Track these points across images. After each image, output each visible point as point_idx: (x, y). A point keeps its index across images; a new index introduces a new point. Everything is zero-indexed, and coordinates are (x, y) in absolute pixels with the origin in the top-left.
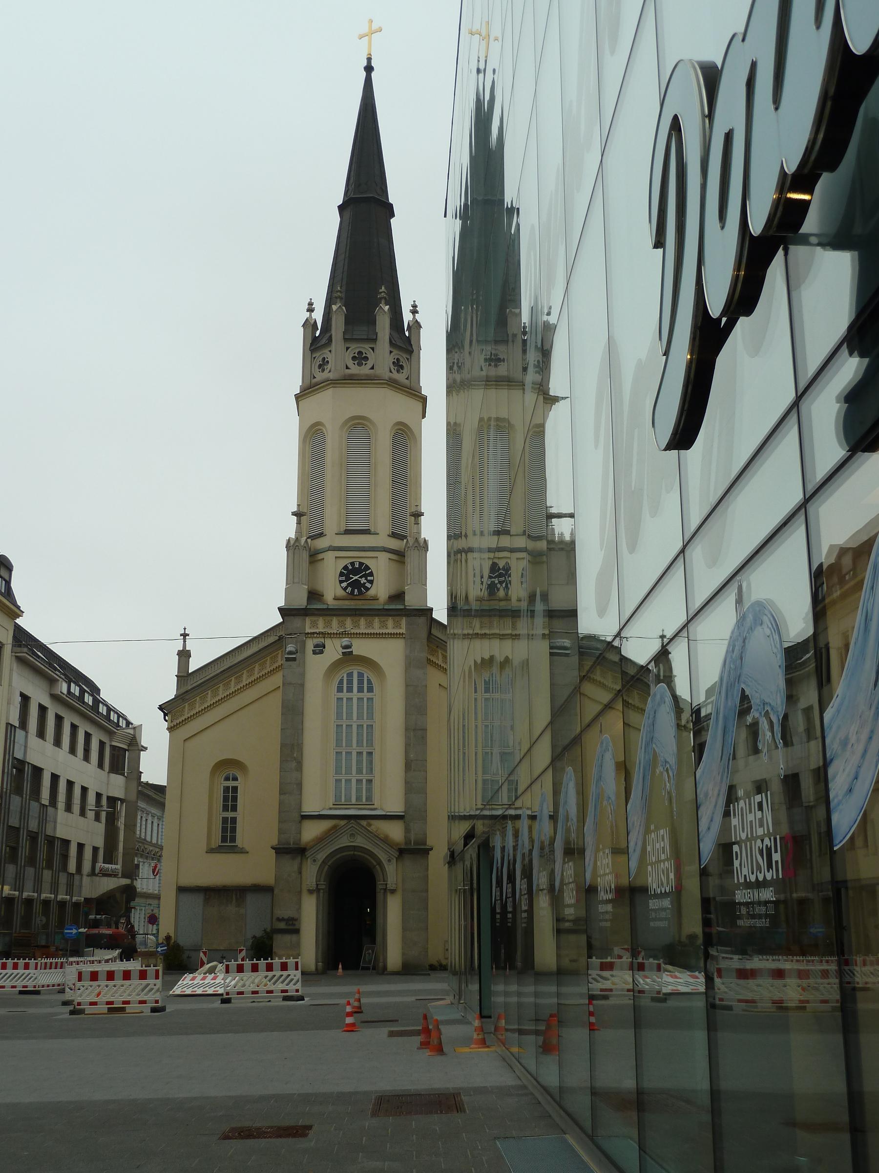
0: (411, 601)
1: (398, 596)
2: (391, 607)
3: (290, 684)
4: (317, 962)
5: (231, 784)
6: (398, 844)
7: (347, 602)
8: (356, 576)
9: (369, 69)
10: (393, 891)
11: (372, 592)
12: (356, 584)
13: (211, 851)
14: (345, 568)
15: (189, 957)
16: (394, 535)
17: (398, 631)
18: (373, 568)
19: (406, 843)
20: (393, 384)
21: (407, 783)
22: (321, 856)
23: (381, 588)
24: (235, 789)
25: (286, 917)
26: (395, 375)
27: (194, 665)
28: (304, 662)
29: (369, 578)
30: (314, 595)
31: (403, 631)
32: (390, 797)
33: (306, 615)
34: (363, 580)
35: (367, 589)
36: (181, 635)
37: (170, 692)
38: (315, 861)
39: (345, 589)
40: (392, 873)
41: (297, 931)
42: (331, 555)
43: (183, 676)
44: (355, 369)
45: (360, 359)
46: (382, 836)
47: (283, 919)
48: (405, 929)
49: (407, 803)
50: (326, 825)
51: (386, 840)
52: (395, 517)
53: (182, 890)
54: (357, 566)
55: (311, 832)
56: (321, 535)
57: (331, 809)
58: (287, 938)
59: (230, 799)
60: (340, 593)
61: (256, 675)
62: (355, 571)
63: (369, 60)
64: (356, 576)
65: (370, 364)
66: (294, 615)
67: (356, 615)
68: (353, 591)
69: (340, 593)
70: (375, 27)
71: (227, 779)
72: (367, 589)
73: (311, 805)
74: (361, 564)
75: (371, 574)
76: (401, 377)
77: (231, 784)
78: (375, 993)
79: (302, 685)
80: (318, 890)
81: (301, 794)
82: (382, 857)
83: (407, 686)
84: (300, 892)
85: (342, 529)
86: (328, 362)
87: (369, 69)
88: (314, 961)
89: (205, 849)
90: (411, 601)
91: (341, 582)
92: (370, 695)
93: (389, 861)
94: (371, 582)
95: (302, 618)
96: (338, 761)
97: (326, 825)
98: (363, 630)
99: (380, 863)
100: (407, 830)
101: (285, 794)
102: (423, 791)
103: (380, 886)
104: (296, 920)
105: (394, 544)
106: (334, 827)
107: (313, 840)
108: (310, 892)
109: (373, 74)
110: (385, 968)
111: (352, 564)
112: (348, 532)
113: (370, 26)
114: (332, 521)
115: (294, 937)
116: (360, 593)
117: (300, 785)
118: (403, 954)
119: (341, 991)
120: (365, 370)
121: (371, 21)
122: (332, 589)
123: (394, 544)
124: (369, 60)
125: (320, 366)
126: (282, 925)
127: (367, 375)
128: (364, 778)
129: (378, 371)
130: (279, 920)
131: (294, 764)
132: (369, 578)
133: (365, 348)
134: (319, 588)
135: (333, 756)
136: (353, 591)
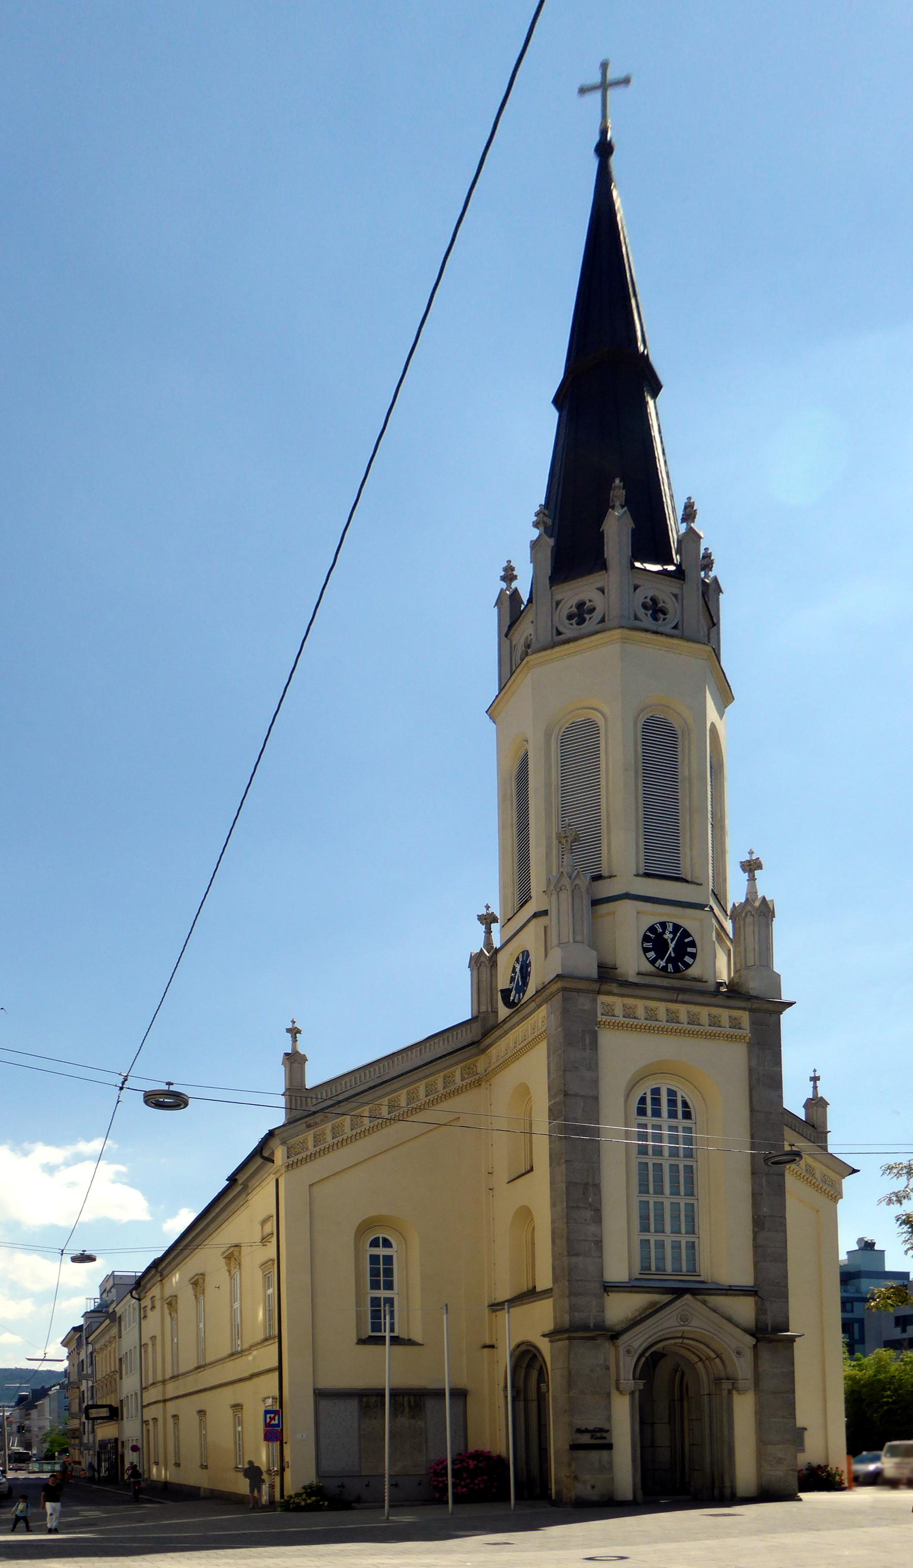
3: (576, 1095)
5: (381, 1251)
9: (604, 149)
13: (361, 1342)
24: (389, 1260)
25: (591, 1428)
27: (313, 1077)
28: (597, 1064)
29: (660, 930)
35: (688, 966)
36: (288, 1030)
38: (628, 1352)
39: (653, 962)
41: (609, 1447)
43: (296, 1093)
47: (586, 1431)
49: (756, 1278)
53: (320, 1395)
55: (619, 1308)
58: (594, 1455)
59: (381, 1272)
69: (647, 967)
70: (611, 75)
71: (375, 1243)
77: (381, 1251)
79: (596, 1098)
81: (601, 1257)
83: (752, 1110)
85: (641, 872)
87: (604, 149)
88: (631, 1491)
89: (355, 1340)
91: (646, 950)
92: (687, 1123)
100: (760, 1311)
101: (577, 1255)
104: (607, 1431)
115: (605, 1453)
126: (585, 1439)
128: (684, 1240)
130: (579, 1431)
132: (660, 930)
134: (609, 960)
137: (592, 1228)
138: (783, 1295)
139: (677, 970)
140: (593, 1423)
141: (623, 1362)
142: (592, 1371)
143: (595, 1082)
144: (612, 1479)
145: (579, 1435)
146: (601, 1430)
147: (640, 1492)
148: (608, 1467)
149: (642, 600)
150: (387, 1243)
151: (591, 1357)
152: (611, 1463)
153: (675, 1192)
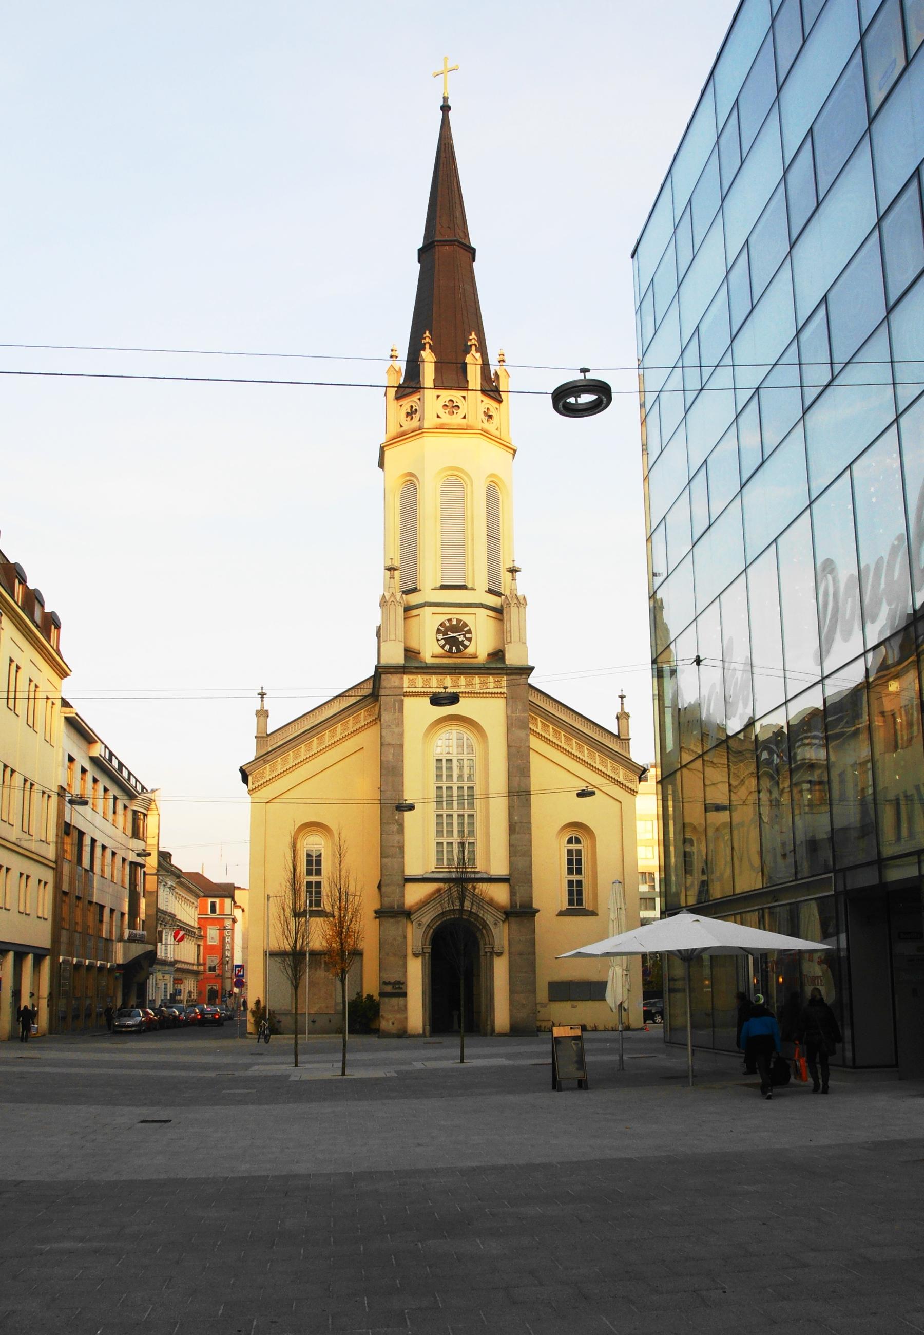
0: (512, 659)
1: (498, 655)
2: (494, 666)
3: (389, 744)
4: (424, 1026)
5: (574, 847)
6: (503, 907)
7: (445, 661)
8: (454, 636)
9: (445, 108)
10: (499, 954)
11: (470, 650)
12: (452, 642)
14: (442, 624)
15: (279, 1022)
16: (490, 591)
17: (499, 690)
18: (472, 626)
19: (512, 906)
20: (485, 433)
21: (511, 845)
22: (427, 919)
23: (480, 646)
25: (393, 981)
26: (487, 426)
29: (467, 636)
30: (410, 653)
31: (504, 690)
32: (494, 858)
33: (404, 673)
34: (461, 638)
35: (466, 647)
37: (249, 753)
38: (420, 924)
39: (443, 647)
40: (501, 934)
41: (404, 995)
42: (428, 610)
43: (263, 738)
44: (446, 419)
45: (452, 407)
46: (487, 899)
47: (389, 983)
48: (512, 992)
49: (511, 865)
50: (430, 887)
51: (491, 903)
52: (493, 575)
54: (454, 622)
55: (414, 895)
56: (415, 590)
57: (433, 872)
58: (394, 1000)
60: (439, 651)
61: (339, 737)
62: (454, 629)
63: (445, 99)
64: (454, 636)
65: (461, 413)
66: (391, 673)
67: (455, 674)
68: (451, 649)
69: (439, 651)
72: (466, 647)
73: (412, 869)
74: (459, 621)
75: (469, 632)
76: (490, 427)
77: (574, 847)
78: (482, 1057)
79: (402, 746)
80: (492, 953)
82: (490, 920)
83: (509, 746)
84: (405, 957)
85: (438, 585)
86: (416, 410)
87: (445, 108)
88: (421, 1025)
90: (512, 659)
93: (495, 924)
94: (470, 640)
95: (399, 676)
96: (439, 824)
97: (430, 887)
98: (477, 688)
99: (485, 925)
100: (512, 893)
102: (528, 854)
103: (484, 948)
104: (403, 983)
105: (493, 601)
106: (439, 890)
107: (417, 904)
108: (416, 955)
109: (451, 114)
110: (493, 1030)
111: (450, 620)
112: (443, 587)
113: (446, 66)
114: (430, 576)
115: (401, 1000)
116: (459, 651)
117: (402, 848)
118: (511, 1017)
119: (442, 1057)
120: (456, 420)
121: (446, 59)
122: (430, 648)
123: (493, 601)
124: (445, 99)
125: (408, 414)
126: (389, 989)
127: (459, 425)
129: (471, 420)
130: (385, 983)
131: (395, 827)
132: (467, 636)
133: (456, 395)
134: (414, 645)
135: (433, 820)
136: (451, 649)
137: (397, 837)
138: (529, 882)
139: (459, 651)
140: (393, 977)
141: (414, 936)
142: (395, 939)
143: (402, 735)
144: (406, 1018)
145: (384, 986)
146: (399, 983)
147: (428, 1027)
148: (405, 1009)
149: (447, 415)
150: (578, 841)
151: (393, 928)
152: (406, 1006)
153: (450, 816)
